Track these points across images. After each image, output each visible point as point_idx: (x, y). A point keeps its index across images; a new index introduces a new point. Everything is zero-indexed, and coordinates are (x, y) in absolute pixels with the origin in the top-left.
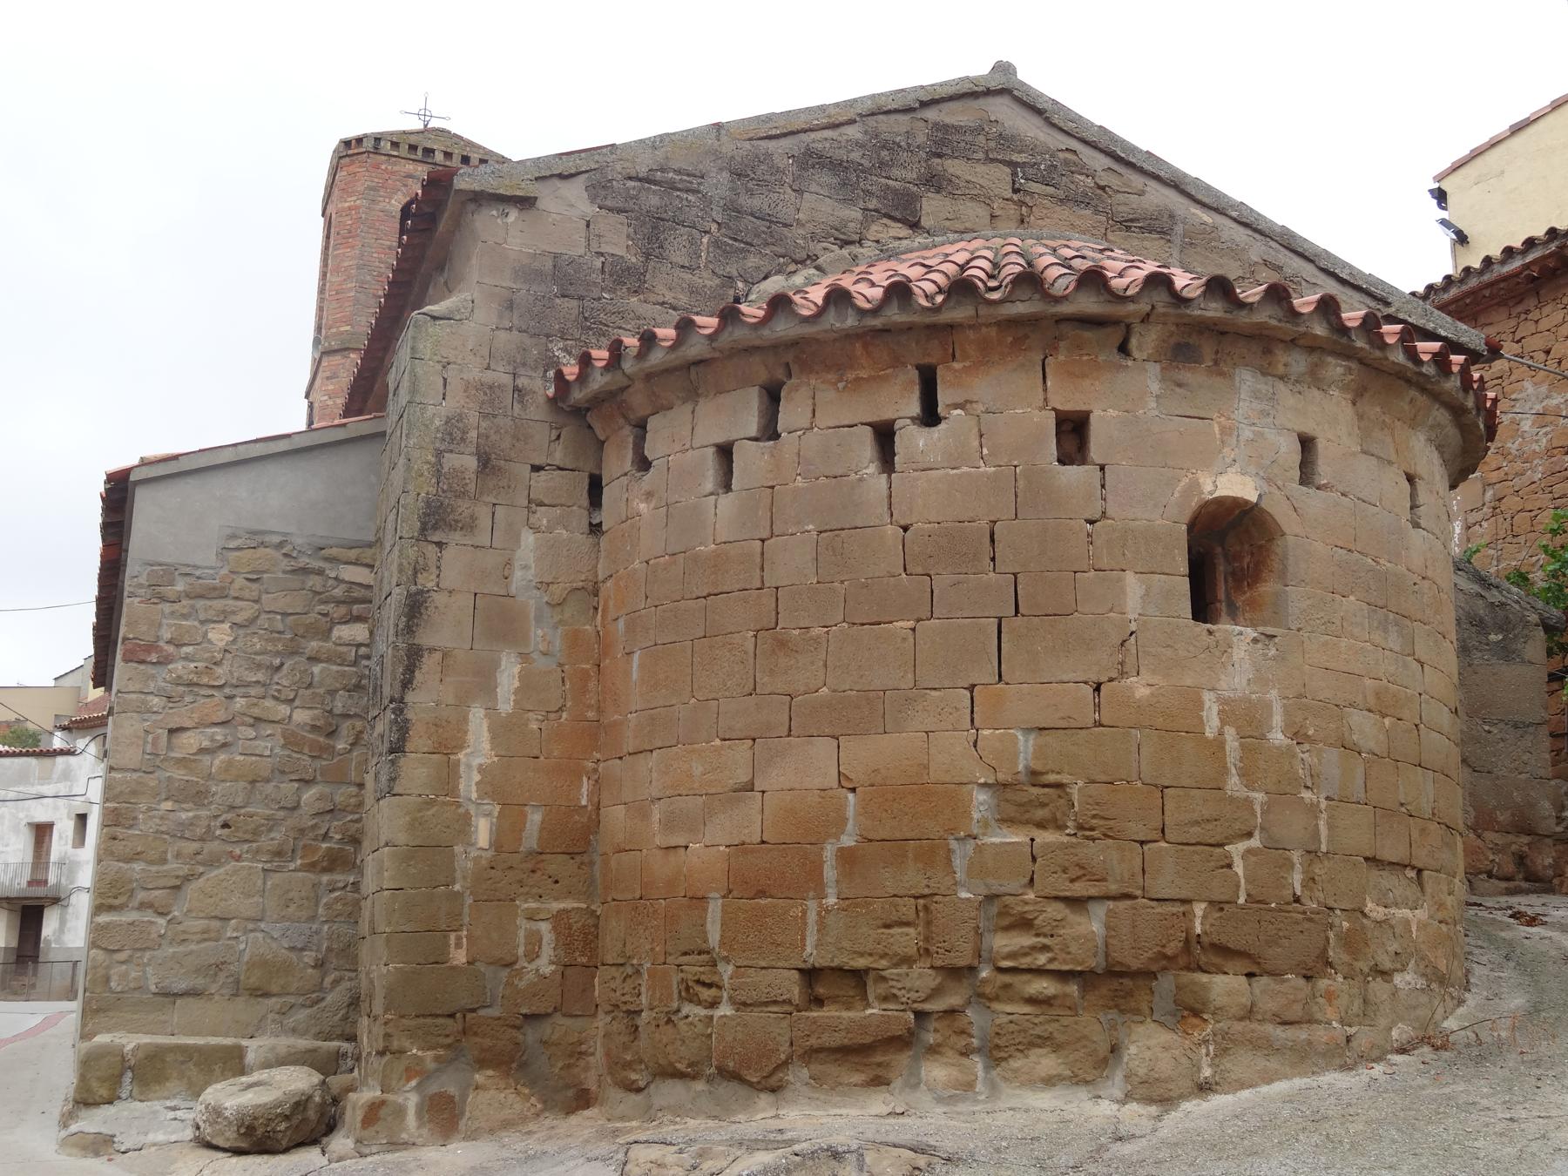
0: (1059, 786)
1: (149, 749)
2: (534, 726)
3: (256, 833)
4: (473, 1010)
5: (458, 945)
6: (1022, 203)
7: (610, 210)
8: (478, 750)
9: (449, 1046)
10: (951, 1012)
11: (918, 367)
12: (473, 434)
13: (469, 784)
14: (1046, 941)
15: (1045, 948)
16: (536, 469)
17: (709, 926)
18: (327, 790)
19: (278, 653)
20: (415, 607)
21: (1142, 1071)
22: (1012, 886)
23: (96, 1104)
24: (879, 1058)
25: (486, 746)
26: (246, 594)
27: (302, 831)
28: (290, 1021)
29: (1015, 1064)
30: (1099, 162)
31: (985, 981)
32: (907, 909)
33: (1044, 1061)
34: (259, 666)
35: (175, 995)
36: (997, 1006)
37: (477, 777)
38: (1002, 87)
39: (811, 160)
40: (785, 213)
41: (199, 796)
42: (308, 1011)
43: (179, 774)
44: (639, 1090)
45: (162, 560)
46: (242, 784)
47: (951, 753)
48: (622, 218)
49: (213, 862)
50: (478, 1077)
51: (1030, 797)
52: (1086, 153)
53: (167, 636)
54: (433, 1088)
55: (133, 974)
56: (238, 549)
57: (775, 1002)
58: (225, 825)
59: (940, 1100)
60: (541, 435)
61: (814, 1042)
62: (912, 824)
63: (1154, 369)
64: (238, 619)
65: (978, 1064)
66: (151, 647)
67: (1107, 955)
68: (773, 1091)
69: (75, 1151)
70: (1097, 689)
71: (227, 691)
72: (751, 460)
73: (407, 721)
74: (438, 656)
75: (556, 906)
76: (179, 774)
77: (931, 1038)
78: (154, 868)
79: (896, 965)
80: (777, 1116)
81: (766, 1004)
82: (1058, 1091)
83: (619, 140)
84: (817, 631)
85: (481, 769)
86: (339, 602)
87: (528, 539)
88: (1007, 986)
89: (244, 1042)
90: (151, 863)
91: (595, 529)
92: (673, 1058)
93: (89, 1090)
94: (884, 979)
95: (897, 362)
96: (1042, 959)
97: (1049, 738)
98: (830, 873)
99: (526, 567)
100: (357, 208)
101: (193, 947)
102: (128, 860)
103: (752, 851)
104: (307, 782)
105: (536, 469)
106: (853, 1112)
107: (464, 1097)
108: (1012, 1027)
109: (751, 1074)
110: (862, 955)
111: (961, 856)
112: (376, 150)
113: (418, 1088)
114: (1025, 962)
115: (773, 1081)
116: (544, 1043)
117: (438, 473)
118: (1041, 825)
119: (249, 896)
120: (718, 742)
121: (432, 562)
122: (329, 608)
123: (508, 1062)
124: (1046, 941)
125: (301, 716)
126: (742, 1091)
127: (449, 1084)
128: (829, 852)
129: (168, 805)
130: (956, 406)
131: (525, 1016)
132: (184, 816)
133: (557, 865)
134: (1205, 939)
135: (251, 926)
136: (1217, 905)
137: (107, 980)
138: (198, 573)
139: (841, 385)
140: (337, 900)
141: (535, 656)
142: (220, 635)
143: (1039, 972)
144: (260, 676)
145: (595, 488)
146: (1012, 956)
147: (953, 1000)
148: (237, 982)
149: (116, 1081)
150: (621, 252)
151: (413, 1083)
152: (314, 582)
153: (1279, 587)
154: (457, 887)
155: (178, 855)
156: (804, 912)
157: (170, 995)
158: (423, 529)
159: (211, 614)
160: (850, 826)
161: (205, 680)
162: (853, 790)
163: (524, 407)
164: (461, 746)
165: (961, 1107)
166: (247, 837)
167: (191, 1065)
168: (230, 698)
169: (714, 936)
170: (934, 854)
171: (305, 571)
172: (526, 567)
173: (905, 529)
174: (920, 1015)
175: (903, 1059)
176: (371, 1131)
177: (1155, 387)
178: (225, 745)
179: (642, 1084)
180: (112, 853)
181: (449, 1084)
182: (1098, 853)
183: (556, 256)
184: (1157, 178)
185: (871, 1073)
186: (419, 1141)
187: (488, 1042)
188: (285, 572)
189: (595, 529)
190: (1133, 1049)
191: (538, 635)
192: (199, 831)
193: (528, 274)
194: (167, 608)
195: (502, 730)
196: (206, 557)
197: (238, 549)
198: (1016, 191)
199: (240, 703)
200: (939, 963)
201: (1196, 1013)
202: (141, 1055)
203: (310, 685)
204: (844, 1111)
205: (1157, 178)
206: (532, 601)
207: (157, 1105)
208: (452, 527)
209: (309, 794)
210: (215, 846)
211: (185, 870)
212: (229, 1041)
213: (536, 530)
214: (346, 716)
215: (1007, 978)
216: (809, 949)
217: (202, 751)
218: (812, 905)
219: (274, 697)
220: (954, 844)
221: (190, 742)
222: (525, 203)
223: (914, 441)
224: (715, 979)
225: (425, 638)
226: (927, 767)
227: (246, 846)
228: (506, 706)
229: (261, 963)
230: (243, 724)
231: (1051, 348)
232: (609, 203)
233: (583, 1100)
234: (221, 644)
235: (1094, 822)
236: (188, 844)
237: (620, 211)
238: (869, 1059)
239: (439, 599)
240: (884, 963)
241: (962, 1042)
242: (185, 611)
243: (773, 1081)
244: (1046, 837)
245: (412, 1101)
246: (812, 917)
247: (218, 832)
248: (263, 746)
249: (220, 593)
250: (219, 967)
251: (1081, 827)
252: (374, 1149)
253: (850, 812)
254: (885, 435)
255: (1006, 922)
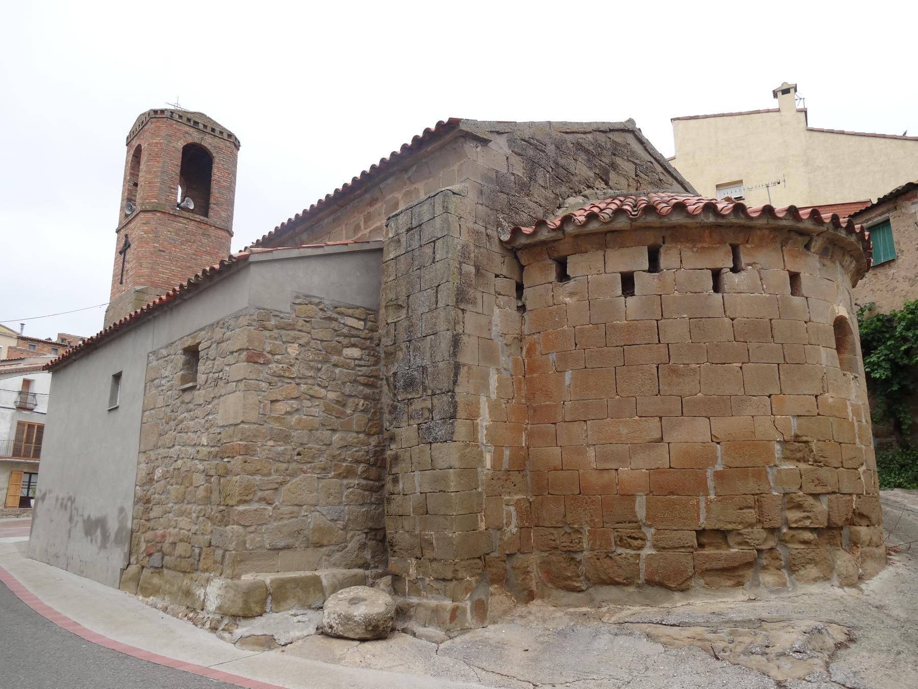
0: (806, 442)
1: (261, 411)
2: (504, 406)
3: (313, 457)
4: (488, 554)
5: (482, 521)
6: (638, 181)
7: (516, 153)
8: (485, 420)
9: (479, 574)
10: (771, 549)
11: (731, 245)
12: (472, 255)
13: (482, 436)
14: (808, 514)
15: (808, 517)
16: (497, 276)
17: (637, 509)
18: (344, 435)
19: (320, 362)
20: (456, 342)
21: (845, 572)
22: (794, 488)
23: (253, 617)
24: (741, 573)
25: (487, 416)
26: (304, 329)
27: (334, 457)
28: (332, 559)
29: (802, 572)
30: (659, 169)
31: (784, 534)
32: (751, 500)
33: (813, 570)
34: (312, 368)
35: (280, 549)
36: (790, 545)
37: (485, 432)
38: (629, 130)
39: (579, 146)
40: (572, 169)
41: (285, 438)
42: (340, 553)
43: (276, 426)
44: (582, 591)
45: (265, 307)
46: (306, 432)
47: (764, 427)
48: (519, 158)
49: (293, 475)
50: (491, 589)
51: (797, 447)
52: (656, 164)
53: (268, 349)
54: (476, 598)
55: (258, 539)
56: (300, 304)
57: (683, 547)
58: (299, 454)
59: (772, 592)
60: (498, 259)
61: (707, 566)
62: (747, 462)
63: (817, 257)
64: (301, 342)
65: (785, 572)
66: (260, 355)
67: (829, 520)
68: (682, 591)
69: (256, 647)
70: (816, 396)
71: (297, 380)
72: (644, 282)
73: (456, 402)
74: (466, 368)
75: (516, 497)
76: (276, 426)
77: (765, 562)
78: (266, 478)
79: (745, 528)
80: (689, 604)
81: (677, 548)
82: (819, 584)
83: (519, 120)
84: (693, 366)
85: (486, 429)
86: (345, 336)
87: (497, 311)
88: (793, 536)
89: (317, 573)
90: (264, 475)
91: (522, 308)
92: (612, 575)
93: (250, 609)
94: (741, 534)
95: (722, 242)
96: (807, 523)
97: (802, 420)
98: (711, 483)
99: (497, 325)
100: (160, 143)
101: (286, 522)
102: (252, 474)
103: (664, 472)
104: (334, 430)
105: (497, 276)
106: (730, 600)
107: (487, 599)
108: (799, 555)
109: (666, 583)
110: (730, 523)
111: (771, 474)
112: (171, 118)
113: (470, 598)
114: (800, 524)
115: (683, 586)
116: (514, 568)
117: (461, 273)
118: (798, 461)
119: (311, 492)
120: (637, 418)
121: (461, 319)
122: (341, 339)
123: (501, 580)
124: (808, 514)
125: (332, 395)
126: (662, 591)
127: (480, 595)
128: (710, 473)
129: (271, 443)
130: (749, 265)
131: (508, 555)
132: (280, 449)
133: (516, 477)
134: (857, 511)
135: (313, 509)
136: (859, 496)
137: (245, 543)
138: (282, 315)
139: (695, 249)
140: (351, 493)
141: (502, 370)
142: (293, 350)
143: (805, 528)
144: (312, 373)
145: (520, 288)
146: (796, 522)
147: (771, 544)
148: (308, 539)
149: (263, 603)
150: (521, 175)
151: (468, 595)
152: (334, 324)
153: (852, 356)
154: (480, 490)
155: (277, 471)
156: (698, 503)
157: (276, 549)
158: (457, 302)
159: (289, 338)
160: (719, 460)
161: (287, 374)
162: (718, 443)
163: (491, 245)
164: (478, 416)
165: (783, 595)
166: (309, 460)
167: (298, 589)
168: (298, 384)
169: (641, 513)
170: (759, 474)
171: (330, 319)
172: (497, 325)
173: (733, 319)
174: (759, 551)
175: (749, 573)
176: (453, 625)
177: (818, 265)
178: (297, 410)
179: (584, 588)
180: (245, 471)
181: (480, 595)
182: (824, 473)
183: (497, 172)
184: (676, 179)
185: (736, 580)
186: (472, 626)
187: (494, 570)
188: (321, 318)
189: (522, 308)
190: (839, 562)
191: (503, 359)
192: (287, 457)
193: (487, 179)
194: (267, 333)
195: (494, 407)
196: (286, 307)
197: (300, 304)
198: (637, 176)
199: (303, 387)
200: (767, 526)
201: (855, 544)
202: (274, 586)
203: (334, 380)
204: (725, 600)
205: (676, 179)
206: (499, 342)
207: (286, 614)
208: (468, 302)
209: (336, 437)
210: (294, 466)
211: (281, 479)
212: (308, 573)
213: (499, 307)
214: (350, 396)
215: (792, 532)
216: (702, 520)
217: (288, 413)
218: (702, 499)
219: (319, 385)
220: (768, 470)
221: (282, 407)
222: (484, 142)
223: (730, 280)
224: (641, 535)
225: (462, 359)
226: (754, 433)
227: (309, 465)
228: (494, 396)
229: (319, 529)
230: (305, 399)
231: (783, 244)
232: (516, 150)
233: (530, 596)
234: (294, 355)
235: (822, 459)
236: (281, 464)
237: (520, 155)
238: (733, 574)
239: (465, 338)
240: (740, 527)
241: (777, 563)
242: (276, 336)
243: (683, 586)
244: (802, 466)
245: (468, 605)
246: (703, 505)
247: (295, 458)
248: (315, 411)
249: (291, 327)
250: (298, 532)
251: (816, 461)
252: (456, 633)
253: (719, 454)
254: (716, 274)
255: (791, 505)
